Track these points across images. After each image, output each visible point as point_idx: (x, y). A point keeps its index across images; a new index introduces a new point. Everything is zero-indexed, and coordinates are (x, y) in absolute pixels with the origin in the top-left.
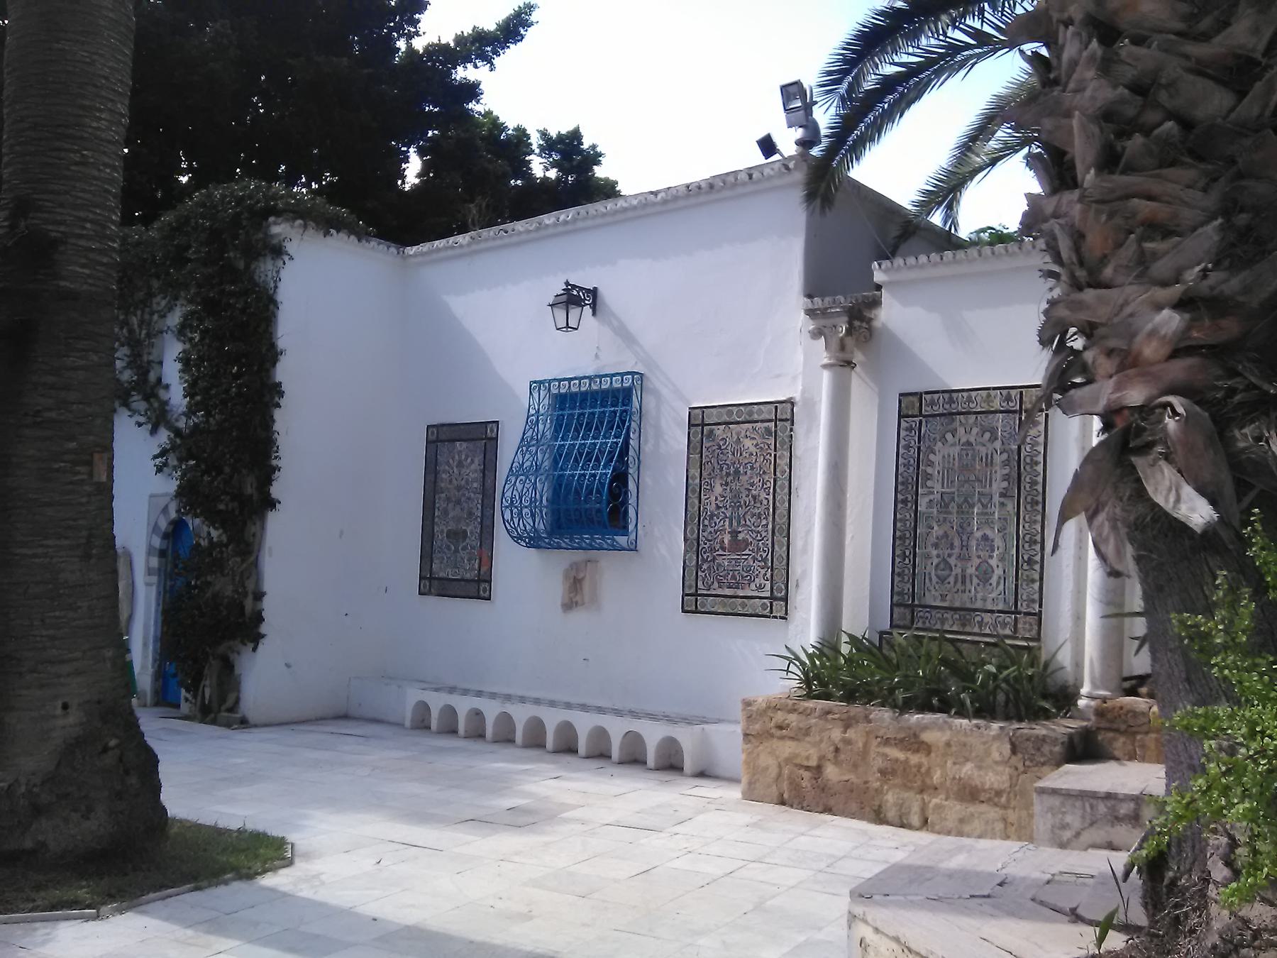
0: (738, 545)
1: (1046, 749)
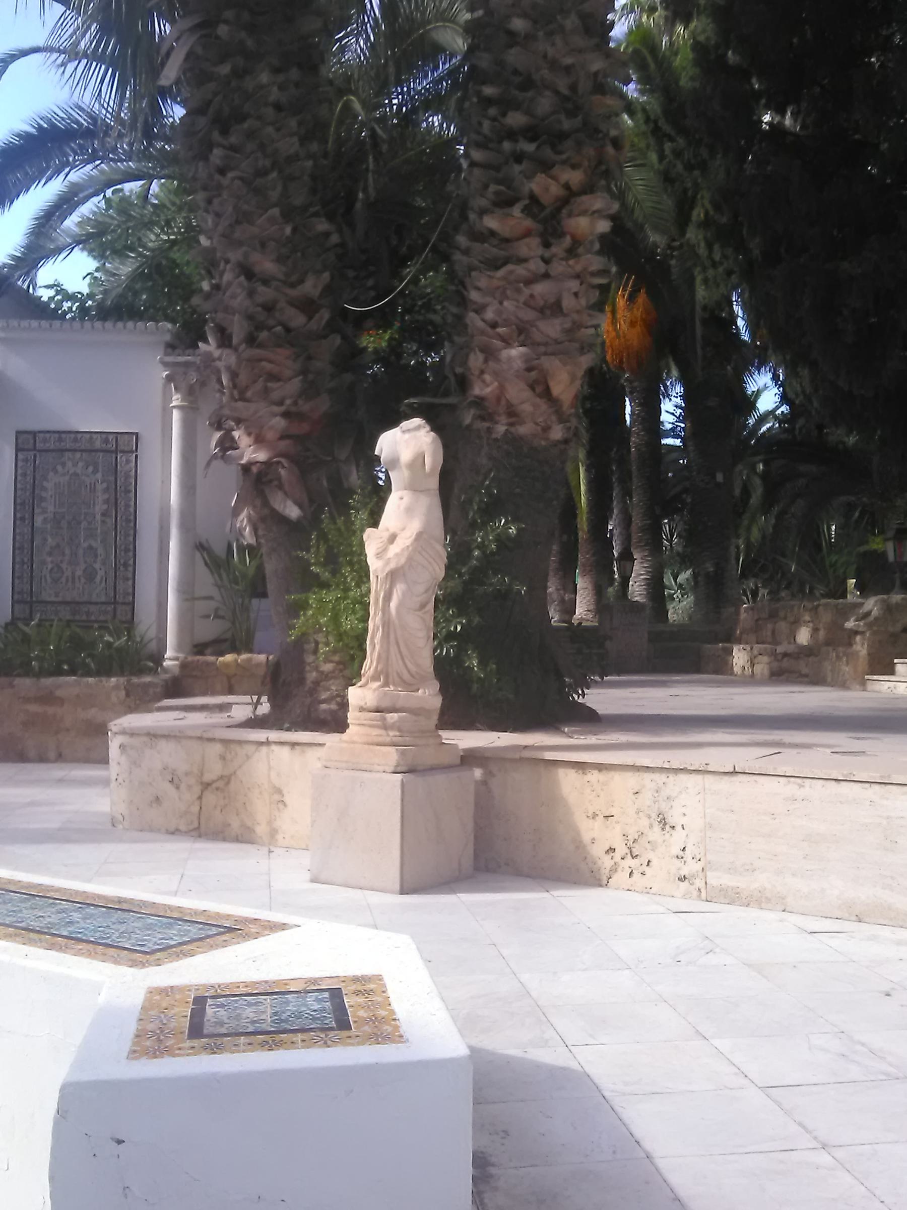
1: (151, 691)
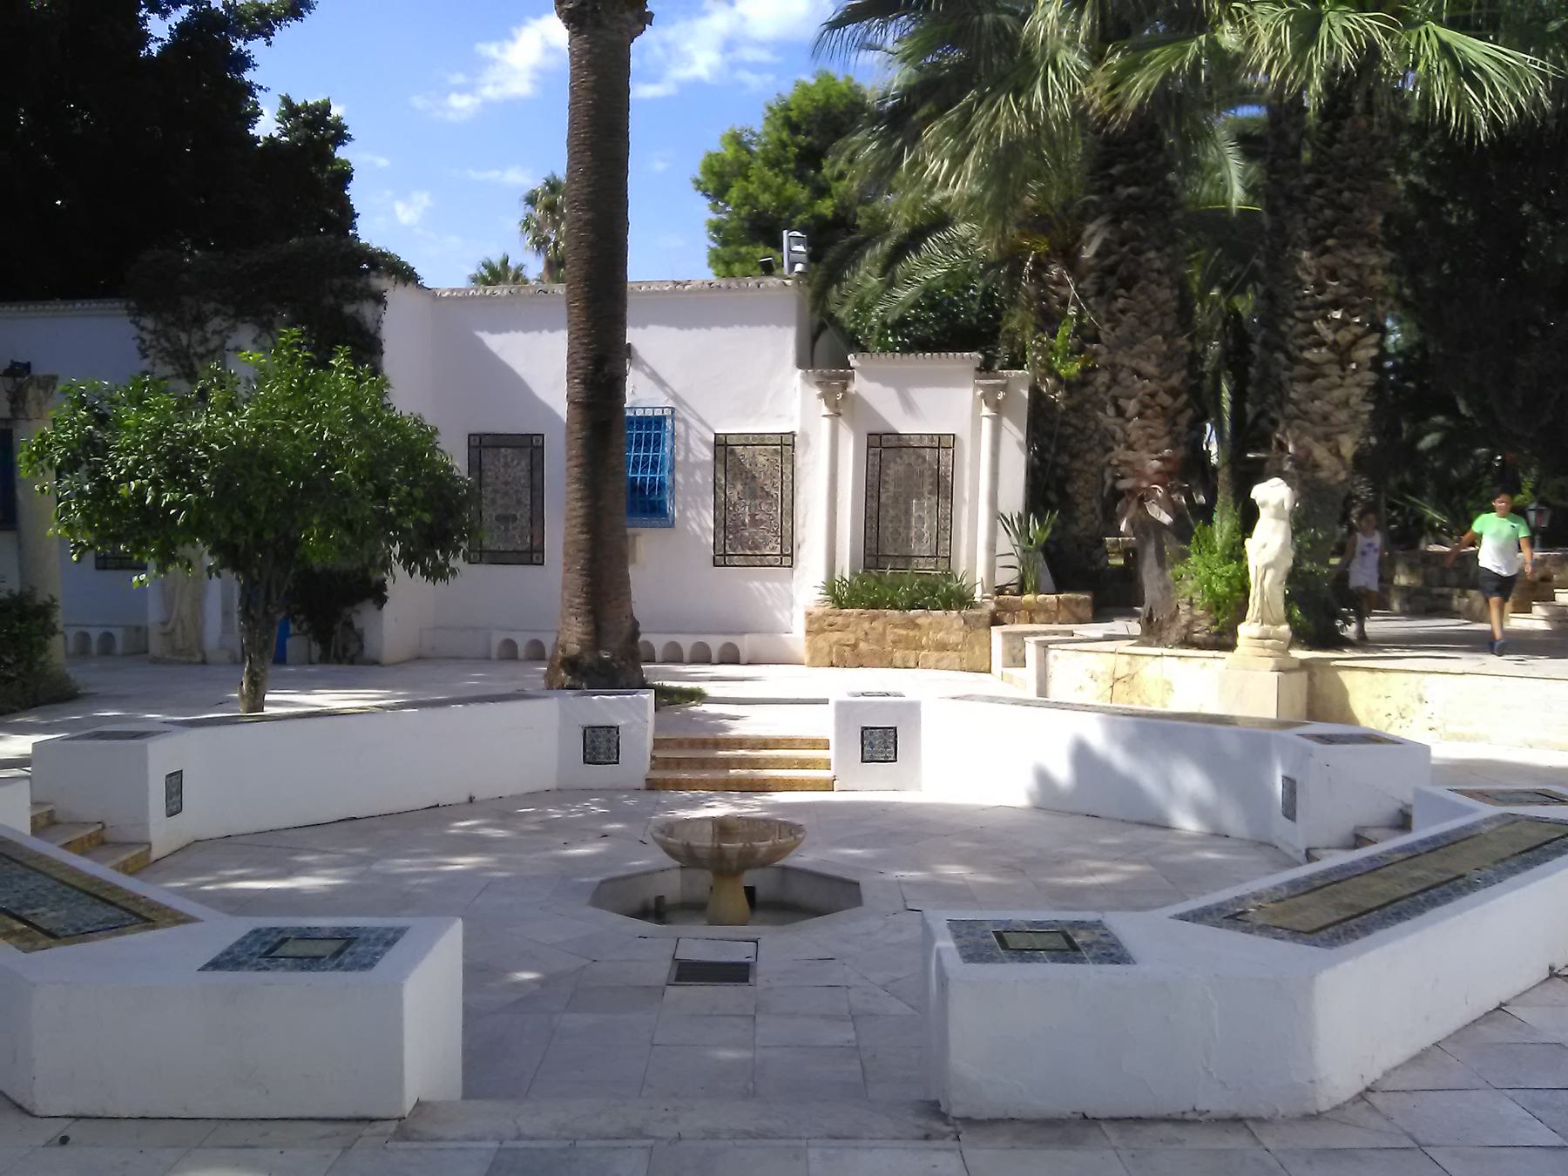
0: (755, 522)
